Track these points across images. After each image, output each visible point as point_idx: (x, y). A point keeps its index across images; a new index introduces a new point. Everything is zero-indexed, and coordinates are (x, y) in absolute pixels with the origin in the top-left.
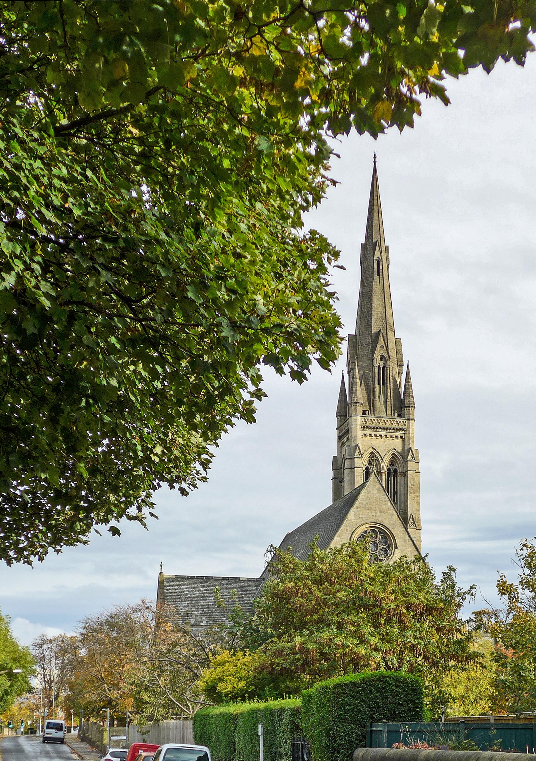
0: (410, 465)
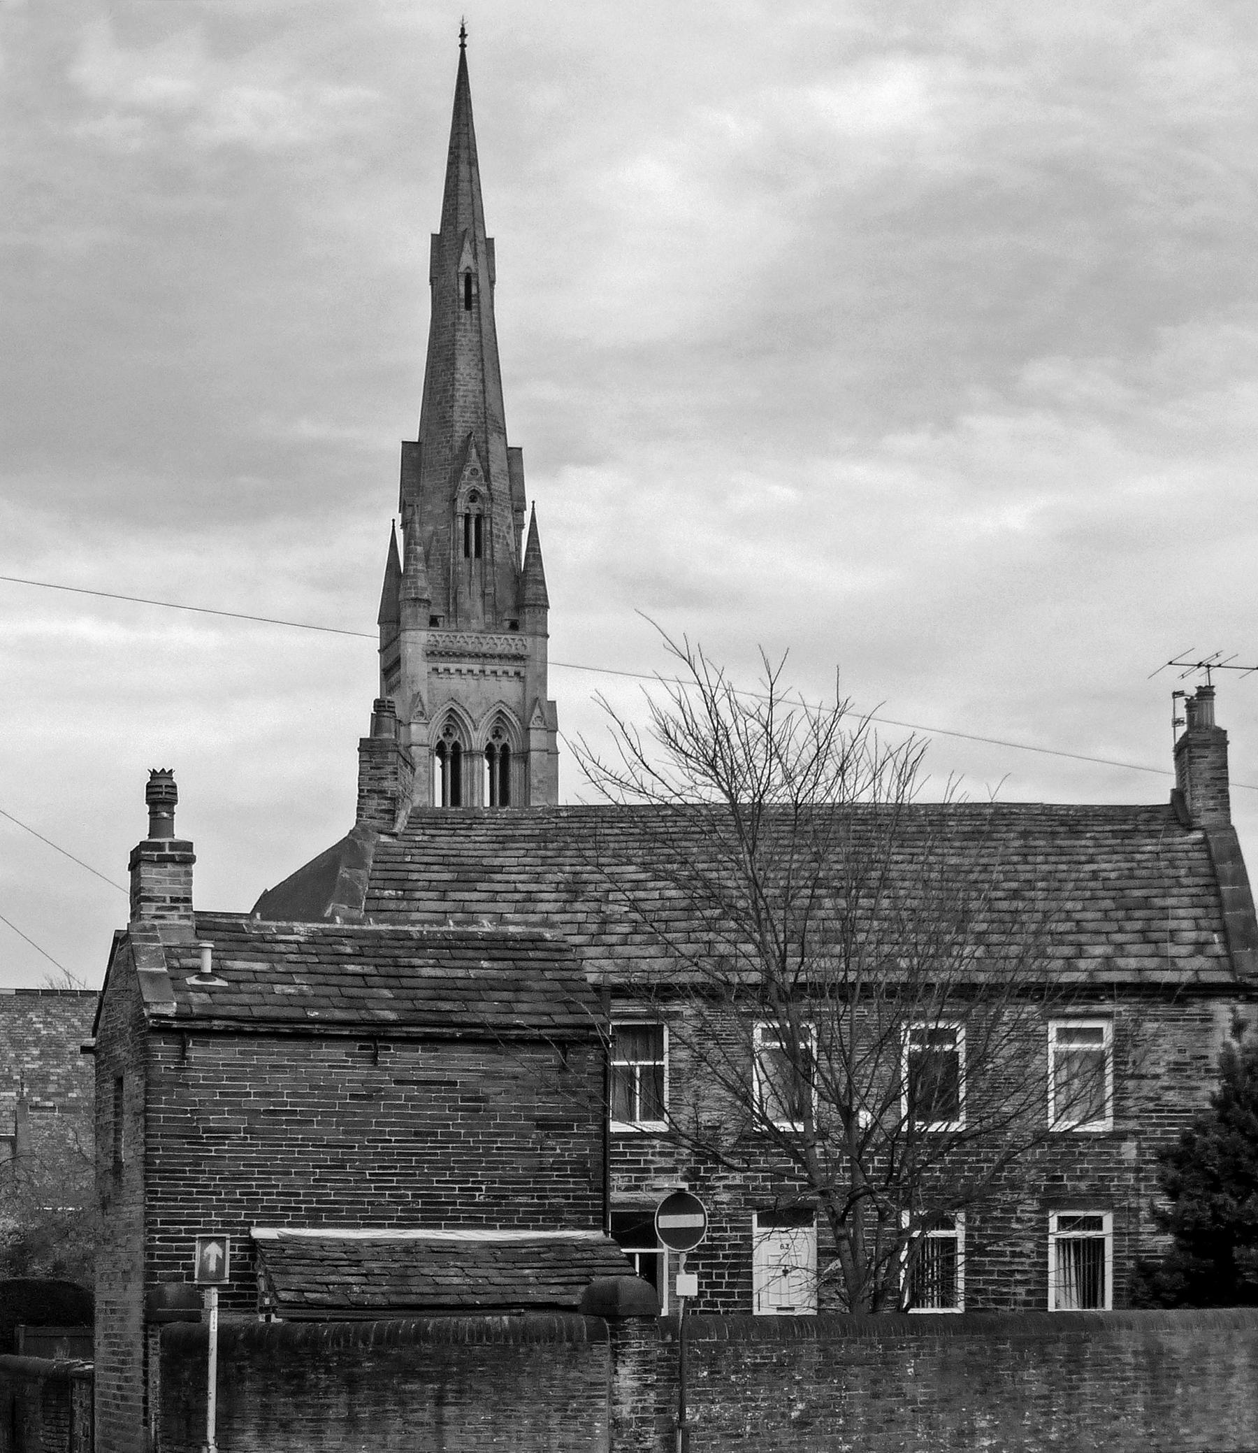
0: (537, 739)
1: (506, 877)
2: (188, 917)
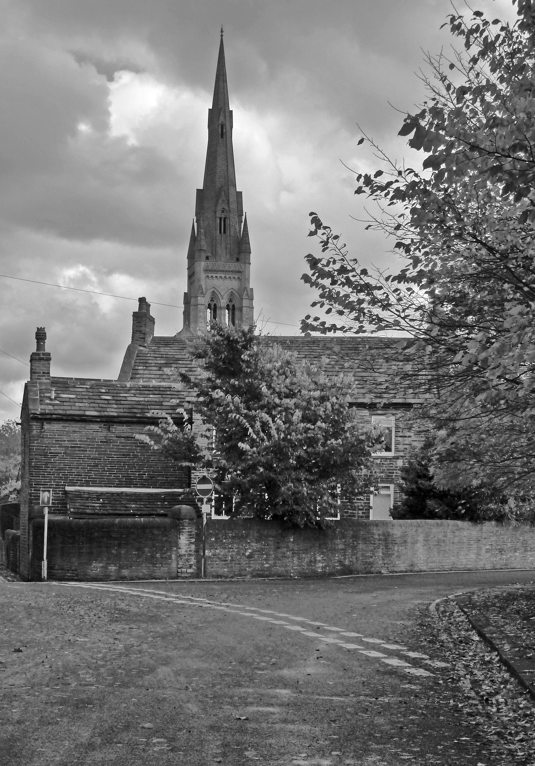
0: (245, 303)
1: (184, 362)
2: (49, 379)
